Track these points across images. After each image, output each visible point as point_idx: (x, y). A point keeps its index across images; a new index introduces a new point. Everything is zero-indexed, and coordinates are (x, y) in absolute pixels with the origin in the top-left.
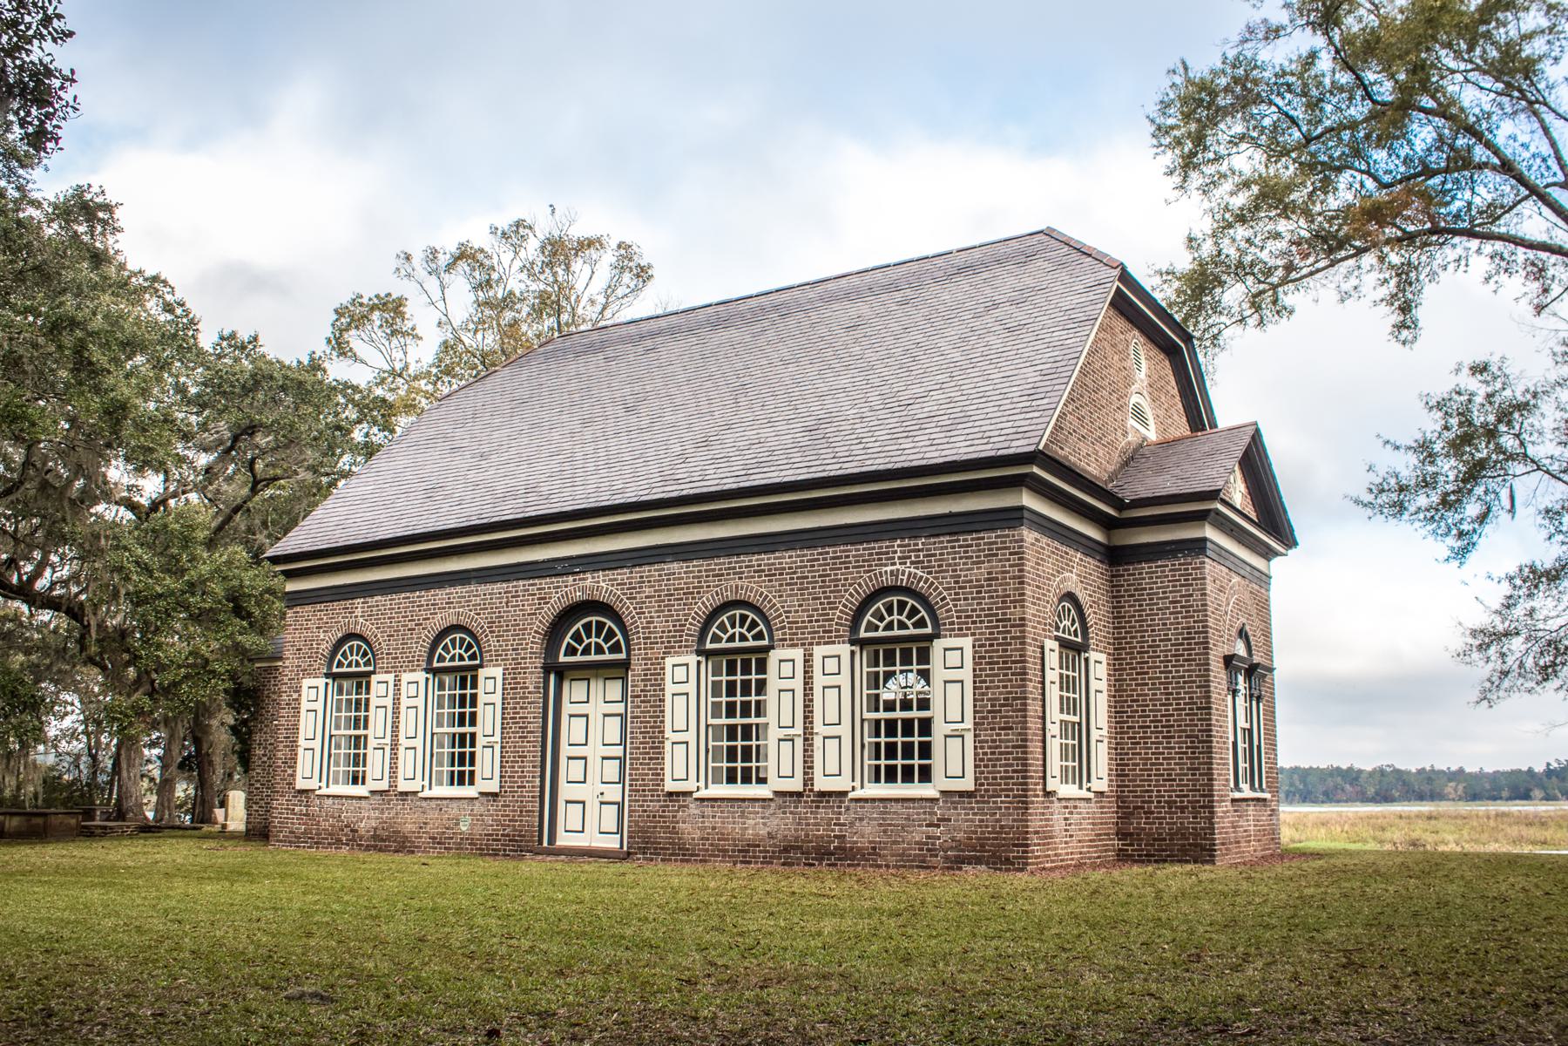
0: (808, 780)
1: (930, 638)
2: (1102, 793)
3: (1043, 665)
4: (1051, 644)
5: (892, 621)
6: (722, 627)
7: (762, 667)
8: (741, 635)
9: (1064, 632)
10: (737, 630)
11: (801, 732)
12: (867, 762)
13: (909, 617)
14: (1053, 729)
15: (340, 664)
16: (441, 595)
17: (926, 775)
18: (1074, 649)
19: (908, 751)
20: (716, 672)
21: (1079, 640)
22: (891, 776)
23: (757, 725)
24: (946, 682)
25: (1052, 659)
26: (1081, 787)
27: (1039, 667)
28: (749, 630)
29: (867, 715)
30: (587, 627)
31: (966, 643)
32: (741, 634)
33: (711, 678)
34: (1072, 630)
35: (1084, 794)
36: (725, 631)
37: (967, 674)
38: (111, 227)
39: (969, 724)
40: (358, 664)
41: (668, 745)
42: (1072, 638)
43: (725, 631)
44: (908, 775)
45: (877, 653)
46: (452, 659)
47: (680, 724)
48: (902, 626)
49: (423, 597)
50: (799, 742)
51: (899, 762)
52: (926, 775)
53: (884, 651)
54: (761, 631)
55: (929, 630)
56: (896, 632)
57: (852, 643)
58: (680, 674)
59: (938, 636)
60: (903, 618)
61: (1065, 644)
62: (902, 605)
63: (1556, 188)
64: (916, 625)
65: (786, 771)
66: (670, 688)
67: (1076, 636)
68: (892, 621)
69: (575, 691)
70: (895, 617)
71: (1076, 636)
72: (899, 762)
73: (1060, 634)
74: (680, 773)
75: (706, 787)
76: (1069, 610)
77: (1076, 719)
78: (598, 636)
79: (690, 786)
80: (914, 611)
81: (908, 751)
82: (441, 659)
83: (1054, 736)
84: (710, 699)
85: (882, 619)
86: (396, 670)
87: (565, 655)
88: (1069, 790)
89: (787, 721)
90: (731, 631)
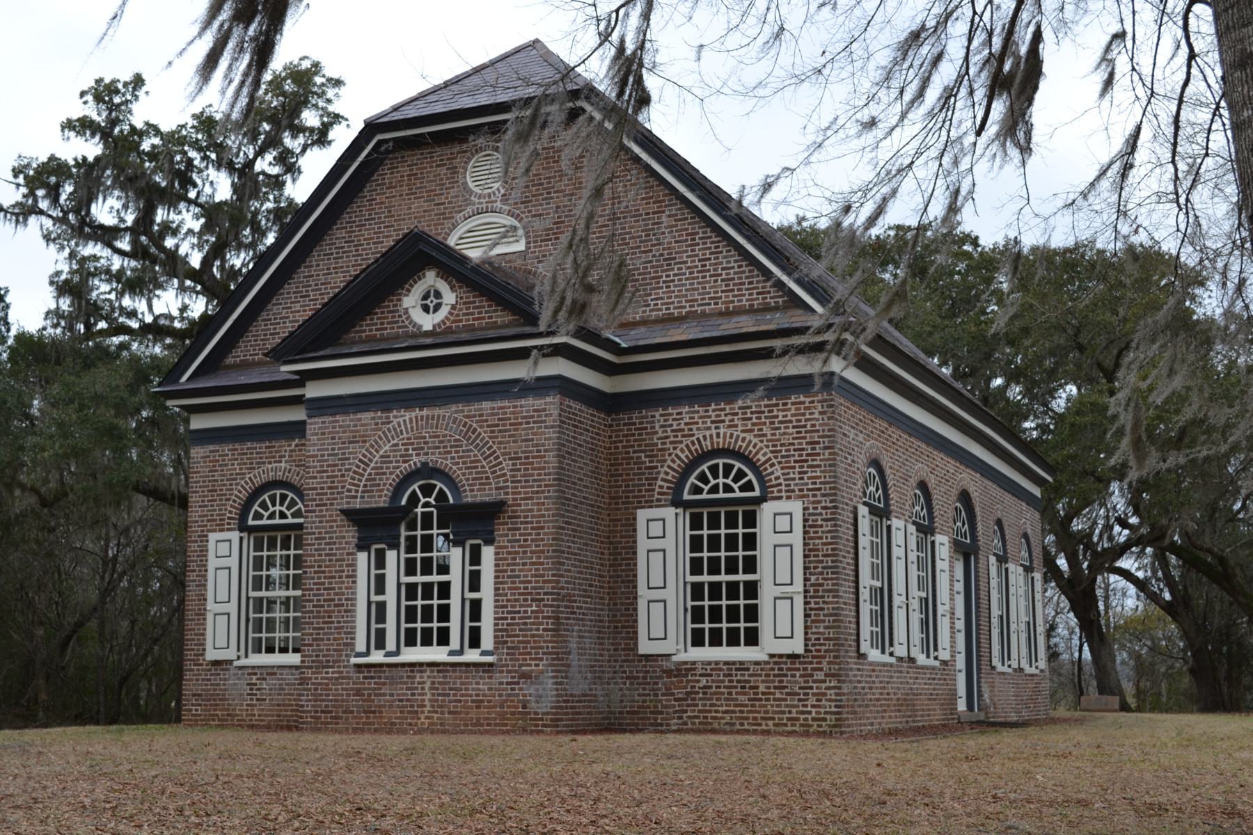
1: (759, 501)
2: (902, 658)
3: (856, 531)
4: (863, 511)
5: (717, 485)
6: (264, 506)
7: (751, 520)
8: (281, 512)
9: (870, 499)
10: (278, 508)
11: (801, 589)
13: (735, 480)
14: (865, 594)
15: (258, 516)
17: (752, 638)
18: (881, 513)
19: (733, 614)
20: (259, 547)
21: (882, 506)
22: (716, 641)
24: (649, 551)
25: (864, 524)
26: (883, 652)
27: (851, 533)
28: (288, 508)
29: (252, 594)
30: (714, 470)
31: (796, 507)
33: (252, 554)
34: (877, 496)
35: (886, 659)
36: (266, 509)
39: (799, 586)
40: (732, 490)
41: (210, 617)
42: (877, 504)
43: (266, 509)
44: (733, 641)
45: (289, 537)
46: (711, 491)
47: (222, 595)
48: (283, 516)
52: (752, 638)
53: (268, 537)
54: (750, 481)
55: (757, 493)
56: (277, 521)
57: (241, 530)
58: (223, 549)
61: (874, 511)
62: (283, 497)
63: (1187, 50)
64: (742, 489)
65: (784, 630)
66: (212, 563)
67: (879, 502)
68: (717, 485)
70: (721, 480)
71: (879, 502)
73: (867, 500)
74: (221, 642)
75: (246, 656)
76: (874, 477)
77: (879, 584)
78: (281, 505)
79: (230, 654)
80: (740, 474)
81: (733, 614)
82: (258, 516)
83: (865, 601)
84: (251, 573)
85: (706, 482)
87: (253, 519)
88: (874, 655)
89: (783, 577)
90: (272, 509)
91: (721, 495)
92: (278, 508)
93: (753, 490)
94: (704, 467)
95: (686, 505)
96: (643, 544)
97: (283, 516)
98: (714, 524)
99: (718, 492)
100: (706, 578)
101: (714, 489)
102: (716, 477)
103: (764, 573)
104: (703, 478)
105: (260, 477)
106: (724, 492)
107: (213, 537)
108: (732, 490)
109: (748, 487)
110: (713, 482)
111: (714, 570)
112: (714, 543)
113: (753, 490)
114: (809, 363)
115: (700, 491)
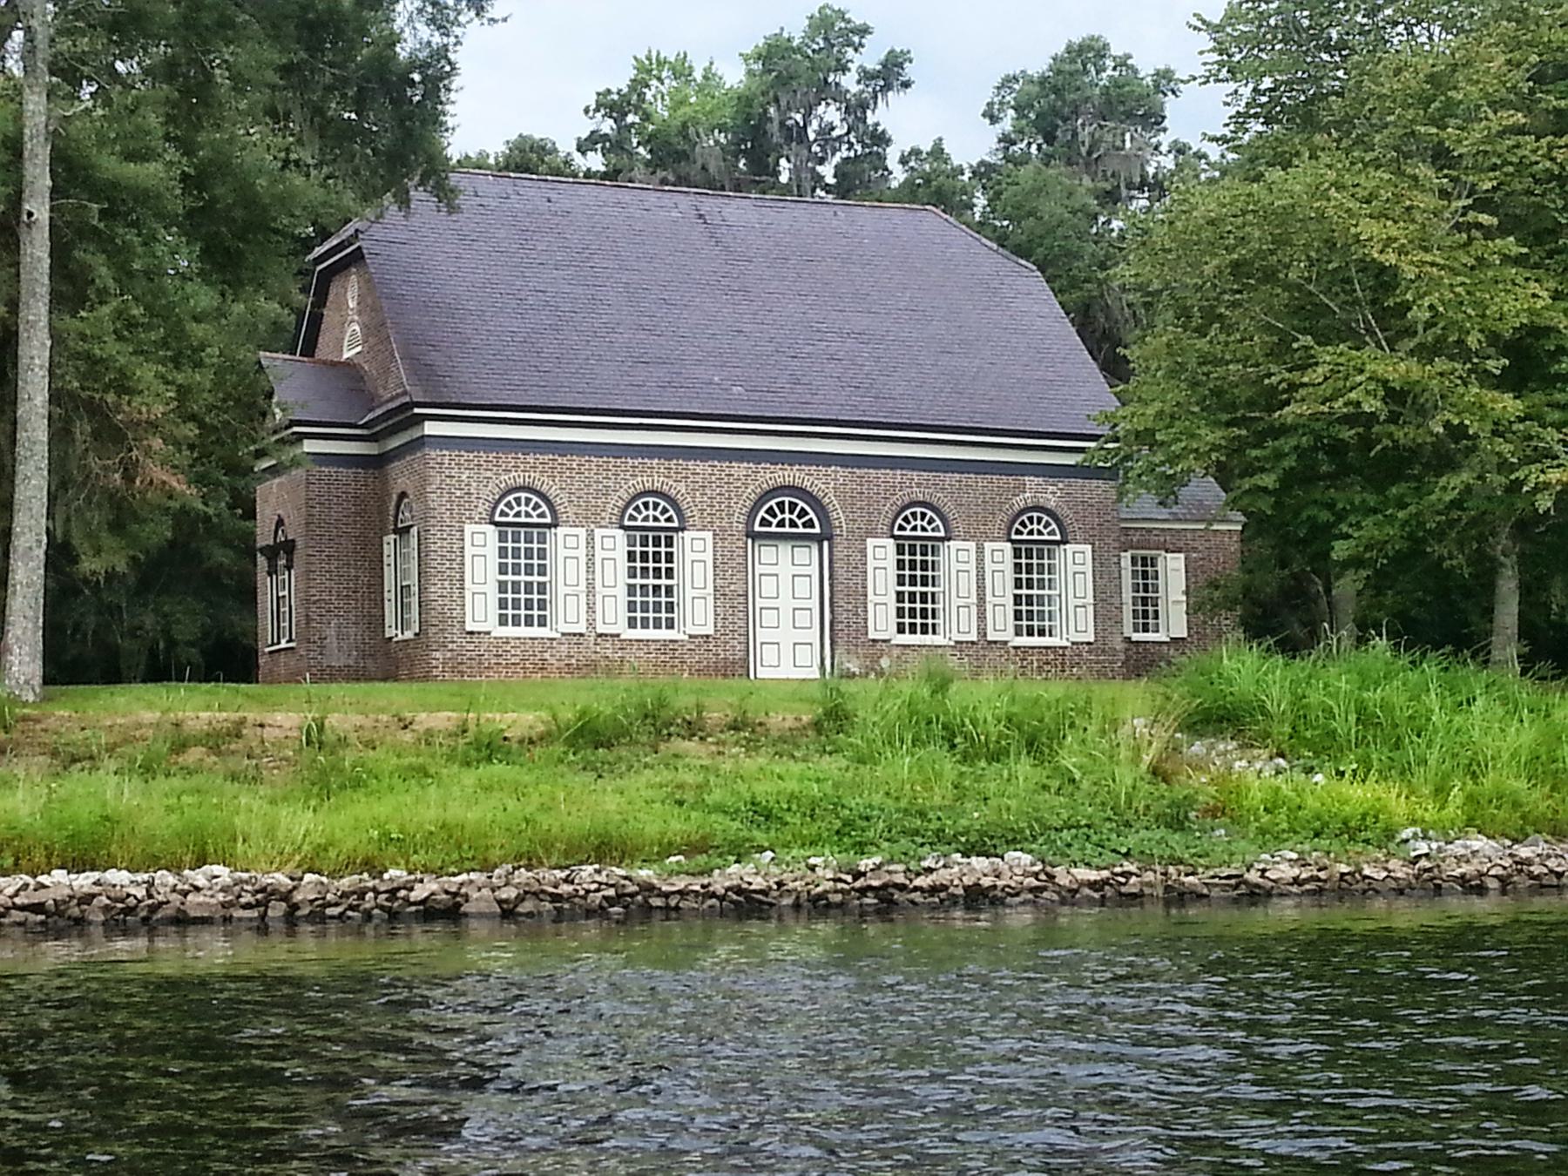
0: (982, 633)
5: (783, 519)
6: (1023, 524)
8: (527, 512)
12: (941, 622)
13: (799, 517)
16: (509, 459)
23: (1049, 596)
30: (781, 505)
32: (791, 520)
37: (1089, 568)
38: (841, 15)
39: (710, 589)
40: (796, 526)
48: (1040, 533)
49: (885, 474)
50: (974, 609)
51: (651, 615)
56: (1035, 537)
59: (683, 529)
60: (794, 517)
64: (804, 525)
68: (783, 519)
69: (767, 553)
70: (787, 516)
72: (651, 615)
80: (665, 511)
85: (908, 522)
86: (980, 538)
91: (787, 529)
92: (787, 516)
93: (673, 521)
94: (773, 503)
95: (497, 524)
96: (469, 551)
97: (1040, 533)
98: (644, 543)
99: (784, 526)
100: (510, 577)
101: (518, 514)
102: (915, 520)
103: (494, 576)
104: (770, 511)
105: (508, 479)
106: (791, 526)
107: (870, 542)
108: (796, 526)
109: (810, 524)
110: (780, 517)
111: (1030, 587)
112: (913, 566)
113: (673, 521)
114: (33, 325)
115: (635, 519)
